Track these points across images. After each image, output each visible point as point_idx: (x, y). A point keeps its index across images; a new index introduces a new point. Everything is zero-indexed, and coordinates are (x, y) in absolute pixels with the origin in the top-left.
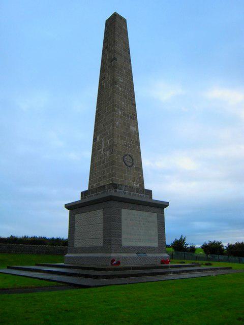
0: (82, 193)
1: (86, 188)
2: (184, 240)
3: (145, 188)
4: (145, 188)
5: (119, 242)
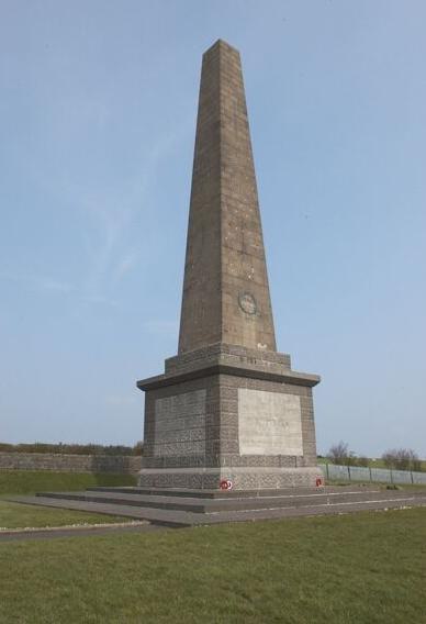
0: (167, 362)
1: (174, 353)
2: (345, 449)
3: (163, 372)
4: (163, 372)
5: (235, 447)
